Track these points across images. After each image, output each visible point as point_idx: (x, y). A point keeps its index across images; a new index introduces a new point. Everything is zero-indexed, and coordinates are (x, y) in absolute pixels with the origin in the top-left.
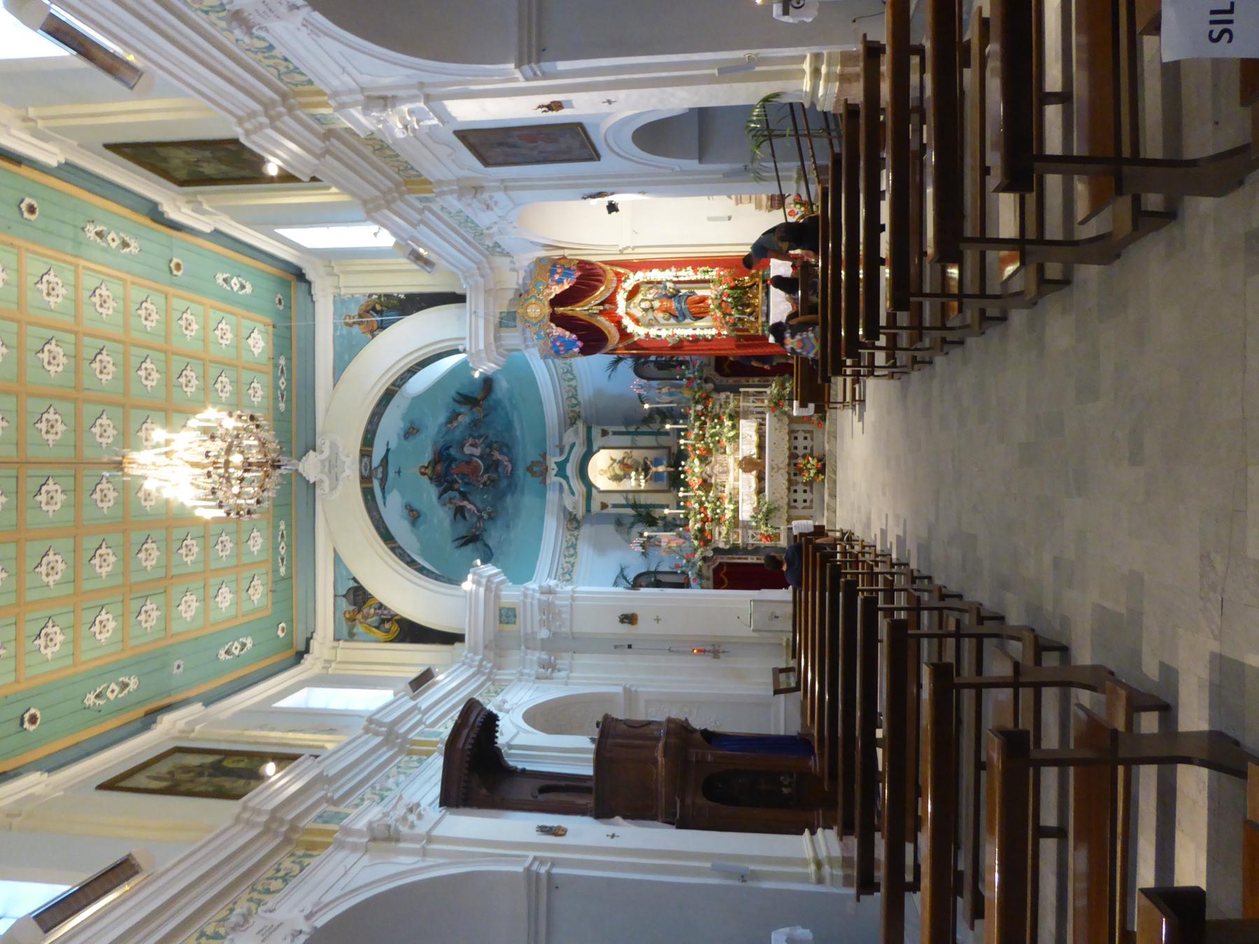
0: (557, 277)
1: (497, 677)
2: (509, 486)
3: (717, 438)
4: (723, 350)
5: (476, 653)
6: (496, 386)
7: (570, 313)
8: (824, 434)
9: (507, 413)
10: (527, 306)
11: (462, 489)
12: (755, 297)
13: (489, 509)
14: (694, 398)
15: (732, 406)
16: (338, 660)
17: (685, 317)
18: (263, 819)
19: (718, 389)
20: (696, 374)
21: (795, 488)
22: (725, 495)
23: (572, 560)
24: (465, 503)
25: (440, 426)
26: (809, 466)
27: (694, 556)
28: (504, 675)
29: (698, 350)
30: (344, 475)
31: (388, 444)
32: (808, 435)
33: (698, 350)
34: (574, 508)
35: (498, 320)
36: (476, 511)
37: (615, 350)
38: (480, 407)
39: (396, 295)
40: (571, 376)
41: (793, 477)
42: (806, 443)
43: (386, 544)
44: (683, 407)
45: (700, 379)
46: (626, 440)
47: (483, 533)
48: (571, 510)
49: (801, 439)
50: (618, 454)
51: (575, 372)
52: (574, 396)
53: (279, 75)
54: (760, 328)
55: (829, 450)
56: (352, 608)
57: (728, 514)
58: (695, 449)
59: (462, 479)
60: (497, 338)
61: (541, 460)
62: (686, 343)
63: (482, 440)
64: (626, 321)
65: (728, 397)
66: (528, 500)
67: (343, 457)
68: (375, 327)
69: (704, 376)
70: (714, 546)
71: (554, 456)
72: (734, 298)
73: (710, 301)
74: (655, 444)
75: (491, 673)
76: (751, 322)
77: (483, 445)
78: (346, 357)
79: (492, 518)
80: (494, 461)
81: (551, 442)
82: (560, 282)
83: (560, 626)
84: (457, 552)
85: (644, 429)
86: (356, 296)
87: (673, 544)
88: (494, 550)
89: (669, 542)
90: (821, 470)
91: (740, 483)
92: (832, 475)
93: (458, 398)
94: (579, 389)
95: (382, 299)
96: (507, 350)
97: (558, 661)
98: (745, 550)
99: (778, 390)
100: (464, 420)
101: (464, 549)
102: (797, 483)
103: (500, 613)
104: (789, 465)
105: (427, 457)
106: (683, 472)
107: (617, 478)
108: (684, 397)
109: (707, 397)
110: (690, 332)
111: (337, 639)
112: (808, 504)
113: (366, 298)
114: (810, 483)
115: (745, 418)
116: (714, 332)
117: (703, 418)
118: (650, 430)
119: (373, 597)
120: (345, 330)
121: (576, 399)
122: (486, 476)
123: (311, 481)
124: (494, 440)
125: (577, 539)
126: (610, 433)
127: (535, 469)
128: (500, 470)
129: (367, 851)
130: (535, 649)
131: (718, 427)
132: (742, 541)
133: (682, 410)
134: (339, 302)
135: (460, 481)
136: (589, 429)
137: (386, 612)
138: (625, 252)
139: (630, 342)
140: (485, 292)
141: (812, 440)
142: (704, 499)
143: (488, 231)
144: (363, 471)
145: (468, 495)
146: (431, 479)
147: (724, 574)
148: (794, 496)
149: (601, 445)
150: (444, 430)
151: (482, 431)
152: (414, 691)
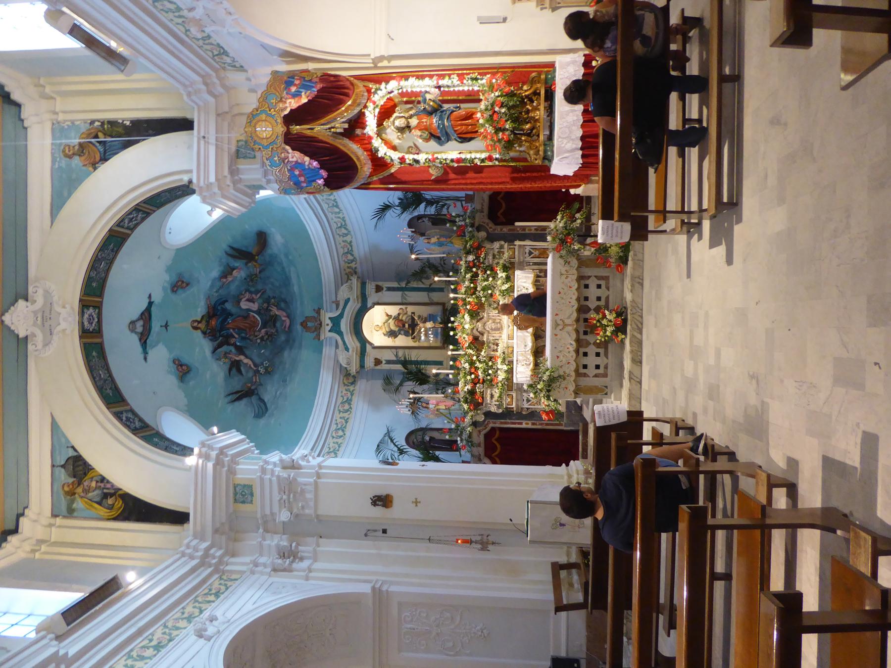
0: (293, 89)
1: (228, 568)
3: (490, 292)
5: (203, 539)
6: (271, 241)
7: (308, 133)
8: (623, 281)
9: (283, 268)
10: (256, 124)
11: (238, 344)
12: (536, 109)
13: (266, 364)
15: (506, 255)
16: (52, 540)
17: (448, 139)
18: (200, 554)
19: (491, 238)
20: (467, 221)
21: (586, 350)
22: (498, 354)
23: (346, 415)
24: (242, 357)
25: (214, 280)
26: (605, 322)
27: (463, 421)
28: (237, 564)
29: (466, 184)
30: (59, 328)
31: (150, 297)
32: (603, 283)
33: (466, 184)
34: (348, 364)
36: (252, 366)
37: (369, 183)
38: (256, 261)
39: (121, 121)
40: (346, 232)
41: (582, 337)
42: (599, 293)
43: (108, 408)
45: (472, 225)
46: (397, 296)
48: (346, 366)
49: (593, 289)
50: (393, 310)
51: (349, 227)
52: (350, 252)
53: (214, 56)
54: (542, 148)
55: (633, 301)
56: (71, 480)
57: (501, 376)
58: (465, 304)
60: (233, 172)
61: (316, 315)
63: (258, 295)
64: (377, 143)
65: (502, 247)
66: (306, 355)
67: (57, 308)
68: (98, 158)
69: (476, 224)
70: (485, 410)
71: (331, 312)
72: (509, 109)
73: (479, 115)
74: (426, 300)
75: (220, 562)
77: (260, 301)
78: (66, 194)
79: (269, 373)
81: (327, 299)
82: (297, 95)
83: (303, 507)
84: (230, 408)
85: (414, 284)
86: (77, 123)
87: (442, 407)
88: (268, 406)
89: (437, 404)
90: (621, 328)
91: (515, 341)
92: (636, 334)
93: (228, 249)
94: (354, 244)
95: (106, 126)
96: (249, 187)
97: (300, 548)
98: (519, 415)
99: (565, 223)
100: (240, 274)
101: (237, 403)
102: (588, 344)
103: (235, 490)
104: (577, 320)
105: (200, 311)
106: (453, 329)
107: (392, 334)
111: (54, 515)
112: (601, 371)
113: (88, 126)
114: (605, 344)
115: (522, 269)
116: (484, 156)
117: (474, 270)
118: (423, 286)
119: (93, 469)
120: (64, 162)
121: (352, 255)
122: (263, 331)
123: (21, 336)
124: (271, 295)
125: (352, 395)
126: (385, 289)
128: (278, 324)
129: (270, 576)
130: (276, 533)
131: (491, 279)
132: (517, 405)
134: (58, 130)
135: (236, 336)
136: (363, 285)
137: (108, 486)
138: (380, 65)
139: (386, 173)
140: (218, 115)
141: (608, 288)
142: (475, 358)
144: (86, 323)
145: (244, 350)
146: (204, 333)
147: (496, 440)
148: (585, 361)
149: (376, 300)
150: (219, 284)
151: (260, 286)
152: (68, 625)
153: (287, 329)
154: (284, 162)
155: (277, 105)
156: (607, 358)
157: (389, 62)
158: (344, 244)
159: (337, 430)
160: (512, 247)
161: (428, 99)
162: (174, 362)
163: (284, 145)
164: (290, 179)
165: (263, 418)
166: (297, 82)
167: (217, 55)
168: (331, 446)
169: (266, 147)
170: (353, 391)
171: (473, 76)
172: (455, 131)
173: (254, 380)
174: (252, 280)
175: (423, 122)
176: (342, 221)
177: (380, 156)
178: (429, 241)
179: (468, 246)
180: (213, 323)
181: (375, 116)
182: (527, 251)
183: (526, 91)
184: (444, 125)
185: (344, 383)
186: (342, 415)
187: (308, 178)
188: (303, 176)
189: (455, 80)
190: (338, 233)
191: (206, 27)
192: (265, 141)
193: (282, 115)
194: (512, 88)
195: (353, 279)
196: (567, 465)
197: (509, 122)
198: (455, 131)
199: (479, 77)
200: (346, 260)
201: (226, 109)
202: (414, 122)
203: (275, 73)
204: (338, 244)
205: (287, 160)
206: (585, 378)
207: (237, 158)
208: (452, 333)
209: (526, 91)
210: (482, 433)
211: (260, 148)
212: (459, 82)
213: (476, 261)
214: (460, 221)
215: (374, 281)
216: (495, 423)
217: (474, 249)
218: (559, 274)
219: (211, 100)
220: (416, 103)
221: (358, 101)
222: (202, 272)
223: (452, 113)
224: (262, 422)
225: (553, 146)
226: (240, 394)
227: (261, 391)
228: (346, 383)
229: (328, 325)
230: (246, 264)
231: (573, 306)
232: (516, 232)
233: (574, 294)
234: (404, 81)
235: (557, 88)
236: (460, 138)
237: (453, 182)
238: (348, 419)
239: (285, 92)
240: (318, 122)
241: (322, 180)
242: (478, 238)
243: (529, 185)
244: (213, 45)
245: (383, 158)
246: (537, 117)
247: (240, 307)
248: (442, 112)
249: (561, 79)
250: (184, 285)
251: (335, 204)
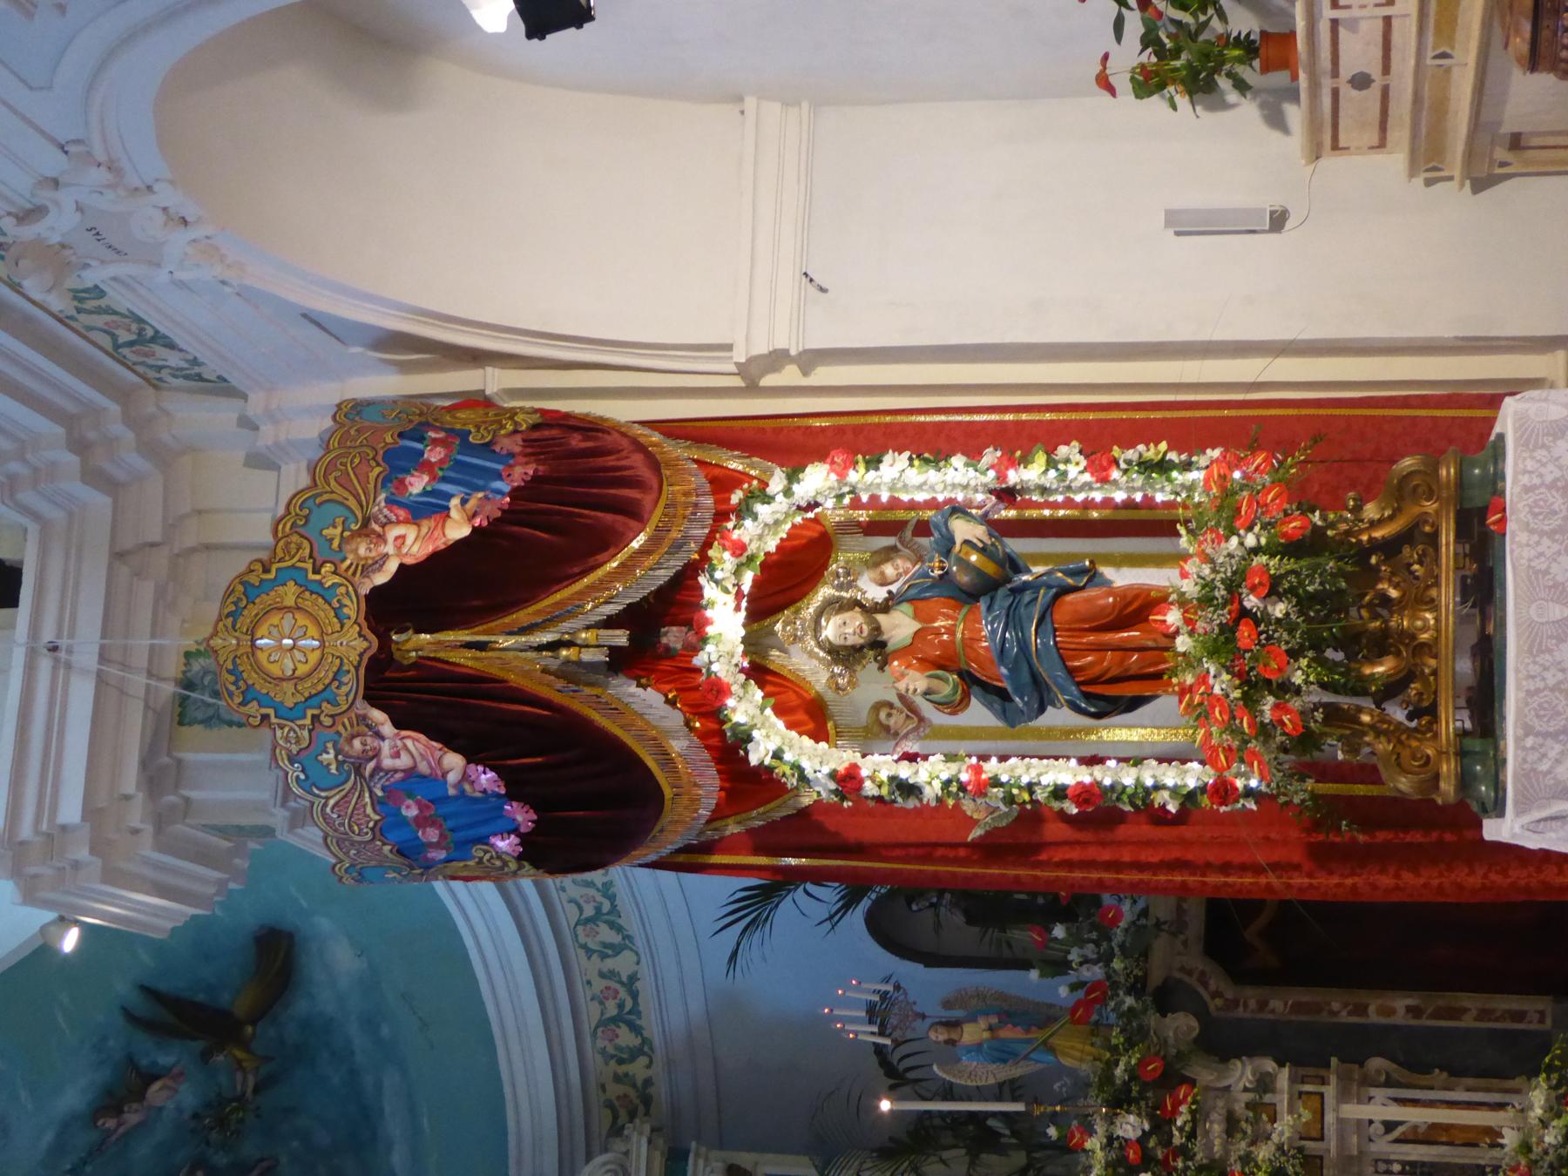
0: (417, 484)
4: (1243, 868)
7: (465, 659)
12: (1421, 599)
14: (1107, 1078)
15: (1284, 1128)
20: (1117, 964)
35: (169, 689)
37: (708, 848)
38: (245, 1046)
40: (607, 935)
44: (1054, 1118)
45: (1137, 988)
51: (631, 922)
52: (629, 1018)
53: (117, 346)
54: (1448, 768)
62: (1054, 831)
65: (1264, 1084)
69: (1156, 978)
72: (1304, 602)
76: (1394, 732)
82: (430, 509)
93: (142, 1007)
94: (645, 987)
96: (223, 831)
108: (1062, 1071)
109: (1172, 1078)
110: (1068, 774)
116: (1194, 775)
121: (635, 1029)
133: (1052, 1132)
138: (768, 381)
139: (778, 810)
140: (118, 556)
143: (28, 232)
154: (358, 771)
155: (347, 547)
157: (805, 373)
158: (605, 983)
160: (1308, 1088)
161: (958, 540)
163: (362, 707)
164: (380, 831)
166: (434, 455)
167: (131, 344)
169: (289, 715)
171: (1151, 453)
172: (1071, 672)
175: (937, 632)
176: (599, 898)
177: (754, 760)
178: (954, 1036)
179: (1119, 1071)
181: (739, 595)
183: (1374, 524)
184: (1023, 645)
187: (452, 830)
188: (433, 823)
189: (1076, 469)
190: (582, 939)
191: (86, 266)
192: (288, 687)
193: (365, 590)
194: (1316, 518)
195: (635, 1138)
197: (1304, 662)
198: (1071, 672)
199: (1173, 456)
200: (611, 1050)
201: (155, 534)
202: (900, 627)
203: (351, 413)
204: (579, 986)
205: (371, 765)
207: (181, 723)
208: (1041, 900)
209: (1374, 524)
211: (265, 717)
212: (1087, 477)
213: (1152, 1143)
214: (1085, 961)
215: (721, 1146)
217: (1145, 1087)
219: (100, 502)
220: (908, 533)
221: (675, 534)
222: (23, 1094)
223: (1057, 597)
225: (1500, 763)
232: (1324, 1018)
234: (861, 468)
235: (1511, 526)
236: (1088, 696)
237: (1058, 855)
239: (382, 496)
240: (507, 620)
241: (513, 839)
242: (1164, 1043)
243: (1386, 881)
244: (115, 313)
245: (770, 770)
246: (1425, 636)
248: (1019, 590)
249: (1527, 489)
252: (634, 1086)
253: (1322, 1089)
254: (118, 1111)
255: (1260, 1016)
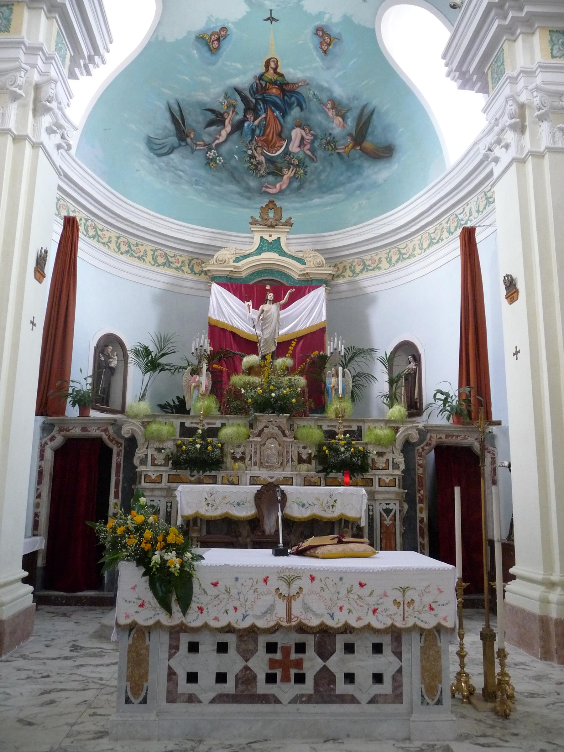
2: (249, 189)
9: (343, 184)
11: (246, 125)
13: (220, 160)
23: (149, 258)
24: (228, 128)
25: (329, 90)
32: (386, 688)
36: (217, 142)
38: (353, 147)
40: (394, 260)
41: (263, 641)
47: (190, 150)
48: (215, 257)
51: (400, 264)
52: (365, 268)
59: (258, 126)
61: (283, 221)
63: (308, 153)
77: (301, 156)
80: (281, 170)
84: (162, 105)
88: (165, 158)
93: (367, 111)
94: (377, 272)
101: (168, 115)
102: (246, 655)
104: (302, 629)
112: (183, 687)
122: (262, 159)
124: (308, 169)
125: (177, 269)
127: (271, 214)
128: (271, 178)
132: (144, 489)
135: (256, 122)
145: (238, 133)
150: (324, 97)
151: (320, 153)
153: (264, 189)
156: (213, 701)
158: (377, 259)
159: (129, 244)
162: (224, 29)
165: (147, 149)
168: (105, 232)
170: (183, 271)
173: (198, 143)
174: (328, 143)
180: (274, 90)
182: (390, 507)
185: (193, 259)
186: (150, 253)
190: (392, 251)
196: (25, 581)
200: (354, 264)
206: (166, 648)
207: (550, 31)
210: (103, 434)
216: (118, 455)
218: (404, 585)
224: (142, 147)
226: (180, 121)
227: (183, 151)
228: (193, 262)
229: (270, 236)
230: (350, 135)
231: (332, 617)
232: (417, 488)
233: (359, 619)
238: (144, 260)
247: (294, 129)
250: (325, 47)
251: (435, 241)
252: (342, 272)
253: (397, 486)
254: (333, 108)
255: (417, 465)
